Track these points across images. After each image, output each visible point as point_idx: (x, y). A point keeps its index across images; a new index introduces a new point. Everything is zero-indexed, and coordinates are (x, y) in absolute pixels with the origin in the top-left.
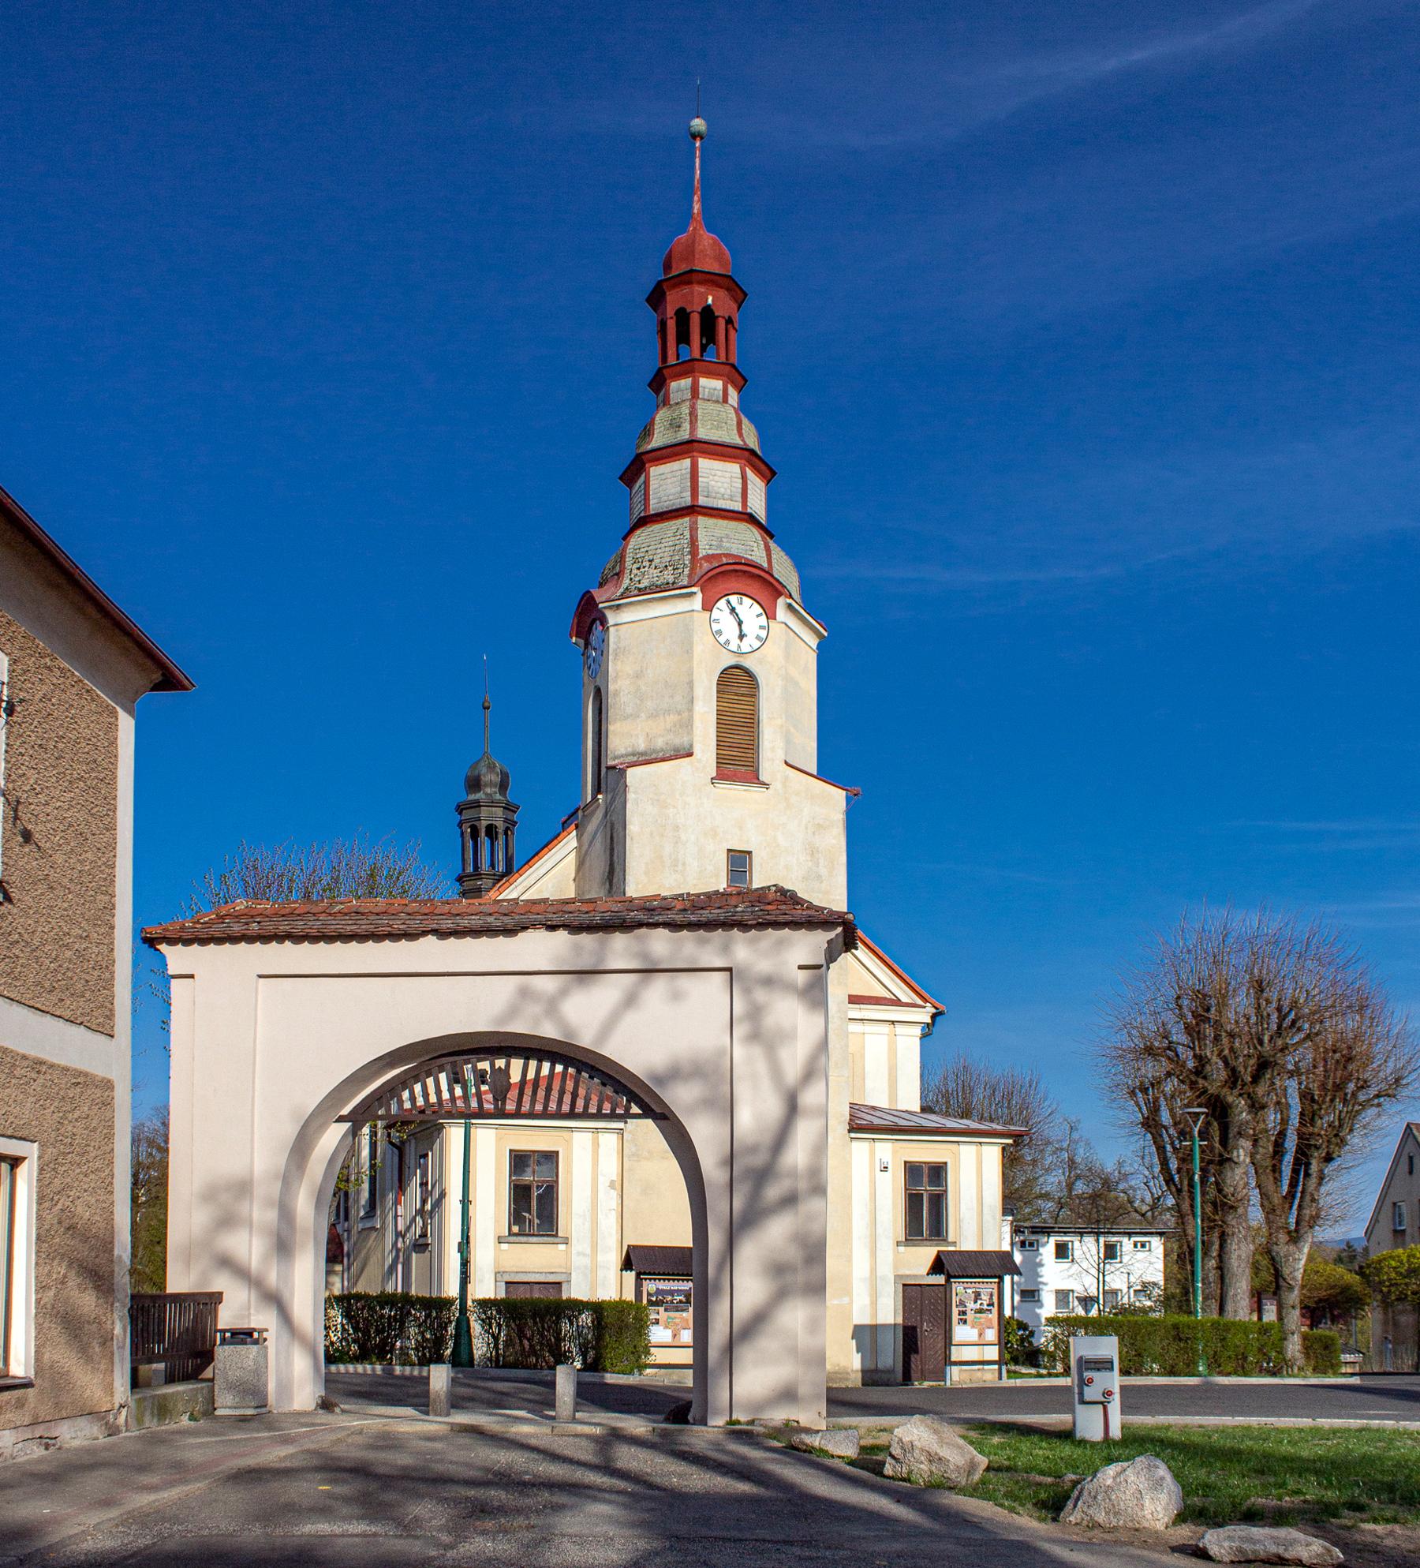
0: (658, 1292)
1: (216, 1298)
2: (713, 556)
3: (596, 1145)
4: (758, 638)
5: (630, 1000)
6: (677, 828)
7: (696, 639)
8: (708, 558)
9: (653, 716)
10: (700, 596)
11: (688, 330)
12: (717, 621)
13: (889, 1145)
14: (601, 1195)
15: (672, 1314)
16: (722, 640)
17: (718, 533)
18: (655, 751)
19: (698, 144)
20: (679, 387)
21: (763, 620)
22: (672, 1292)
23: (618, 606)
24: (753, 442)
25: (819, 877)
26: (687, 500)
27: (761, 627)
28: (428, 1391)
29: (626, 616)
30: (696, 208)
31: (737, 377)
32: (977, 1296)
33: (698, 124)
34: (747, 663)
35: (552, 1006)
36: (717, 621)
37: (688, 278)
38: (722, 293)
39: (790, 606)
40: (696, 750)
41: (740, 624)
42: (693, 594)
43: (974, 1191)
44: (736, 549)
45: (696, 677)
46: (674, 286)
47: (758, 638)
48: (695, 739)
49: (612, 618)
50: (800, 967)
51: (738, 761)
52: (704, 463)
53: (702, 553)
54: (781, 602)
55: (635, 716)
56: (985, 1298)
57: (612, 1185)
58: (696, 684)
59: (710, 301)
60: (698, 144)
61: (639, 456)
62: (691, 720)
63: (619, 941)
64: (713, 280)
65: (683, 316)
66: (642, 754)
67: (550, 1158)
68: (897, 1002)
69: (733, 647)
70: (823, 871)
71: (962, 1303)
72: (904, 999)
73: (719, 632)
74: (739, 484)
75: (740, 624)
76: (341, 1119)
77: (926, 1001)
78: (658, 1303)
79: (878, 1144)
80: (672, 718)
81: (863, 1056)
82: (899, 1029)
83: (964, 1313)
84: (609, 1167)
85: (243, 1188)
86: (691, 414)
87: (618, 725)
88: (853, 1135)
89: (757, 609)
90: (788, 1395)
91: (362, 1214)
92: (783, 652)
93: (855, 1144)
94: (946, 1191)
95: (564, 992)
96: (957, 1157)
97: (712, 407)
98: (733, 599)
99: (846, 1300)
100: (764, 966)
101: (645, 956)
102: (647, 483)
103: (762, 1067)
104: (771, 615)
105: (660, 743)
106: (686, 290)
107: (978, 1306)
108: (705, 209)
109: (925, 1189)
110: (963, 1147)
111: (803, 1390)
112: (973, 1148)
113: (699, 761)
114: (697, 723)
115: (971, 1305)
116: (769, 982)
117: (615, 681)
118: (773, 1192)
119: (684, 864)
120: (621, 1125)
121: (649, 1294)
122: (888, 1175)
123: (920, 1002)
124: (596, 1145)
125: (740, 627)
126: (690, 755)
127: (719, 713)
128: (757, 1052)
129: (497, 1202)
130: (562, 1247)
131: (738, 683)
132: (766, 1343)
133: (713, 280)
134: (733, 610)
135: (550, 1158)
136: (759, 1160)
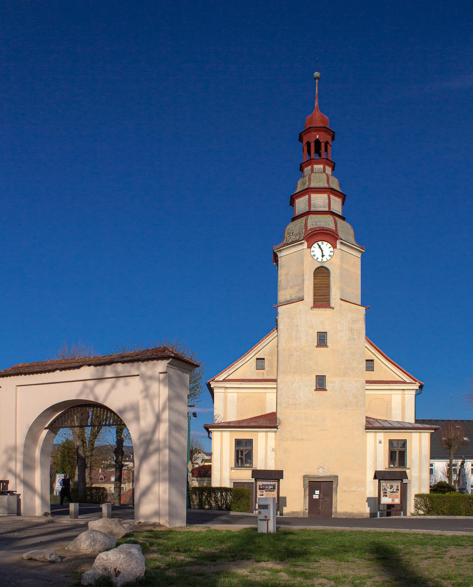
1: (7, 482)
2: (313, 228)
3: (267, 437)
4: (330, 256)
5: (113, 386)
6: (297, 326)
7: (305, 259)
8: (311, 229)
9: (292, 287)
10: (306, 244)
11: (317, 151)
12: (313, 251)
13: (382, 434)
14: (269, 453)
15: (268, 493)
16: (315, 258)
17: (316, 220)
18: (292, 300)
19: (317, 81)
20: (307, 170)
21: (332, 249)
22: (268, 485)
23: (280, 250)
24: (335, 185)
25: (354, 339)
27: (331, 252)
28: (69, 510)
29: (283, 253)
30: (316, 104)
31: (328, 162)
32: (391, 487)
33: (317, 74)
34: (325, 265)
35: (92, 389)
36: (313, 251)
37: (309, 130)
38: (323, 133)
39: (341, 243)
40: (305, 298)
42: (302, 243)
43: (418, 450)
44: (323, 225)
45: (305, 272)
46: (305, 135)
47: (330, 256)
48: (305, 294)
50: (160, 373)
51: (322, 300)
52: (313, 196)
53: (309, 228)
54: (338, 241)
55: (286, 288)
56: (395, 488)
58: (305, 275)
59: (318, 137)
60: (317, 81)
62: (303, 287)
63: (109, 368)
64: (318, 129)
66: (288, 301)
67: (250, 442)
68: (405, 382)
69: (320, 260)
71: (385, 489)
72: (408, 381)
73: (314, 255)
74: (327, 201)
75: (322, 251)
76: (46, 428)
77: (416, 381)
78: (263, 489)
79: (378, 434)
80: (297, 288)
81: (391, 402)
82: (406, 392)
83: (386, 493)
84: (272, 443)
85: (15, 449)
86: (309, 179)
88: (367, 431)
89: (329, 245)
90: (157, 514)
92: (342, 261)
93: (368, 434)
94: (406, 450)
95: (95, 385)
97: (319, 174)
98: (320, 243)
99: (363, 489)
100: (149, 373)
101: (116, 372)
103: (149, 407)
104: (334, 247)
105: (294, 297)
106: (309, 135)
107: (392, 490)
108: (320, 104)
109: (397, 449)
110: (413, 434)
111: (162, 512)
112: (373, 434)
113: (306, 302)
114: (305, 288)
115: (389, 490)
116: (151, 378)
118: (152, 448)
119: (300, 338)
121: (259, 486)
122: (382, 445)
123: (414, 382)
124: (267, 437)
125: (322, 252)
126: (303, 300)
127: (314, 284)
128: (147, 401)
131: (322, 273)
132: (151, 497)
133: (318, 129)
134: (320, 247)
135: (250, 442)
136: (148, 437)
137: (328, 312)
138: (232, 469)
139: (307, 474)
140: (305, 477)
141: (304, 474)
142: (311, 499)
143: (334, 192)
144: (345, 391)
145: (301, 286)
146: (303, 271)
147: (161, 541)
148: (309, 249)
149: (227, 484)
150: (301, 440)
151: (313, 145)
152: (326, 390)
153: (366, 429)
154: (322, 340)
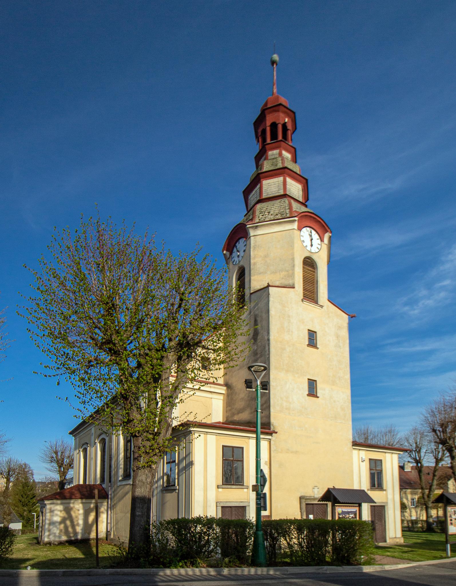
0: (343, 513)
6: (289, 316)
9: (274, 273)
22: (348, 513)
23: (257, 226)
26: (282, 192)
29: (259, 232)
34: (314, 257)
41: (312, 240)
42: (294, 221)
45: (295, 256)
46: (271, 112)
49: (252, 233)
57: (266, 463)
61: (259, 174)
65: (274, 126)
70: (341, 345)
73: (303, 241)
75: (312, 240)
87: (256, 276)
88: (354, 447)
91: (120, 478)
96: (385, 457)
102: (261, 189)
106: (276, 114)
113: (297, 291)
117: (255, 258)
119: (292, 332)
120: (270, 437)
121: (339, 514)
122: (364, 462)
126: (294, 288)
129: (217, 469)
130: (245, 490)
137: (317, 310)
138: (218, 487)
139: (303, 494)
140: (301, 498)
141: (300, 495)
142: (420, 463)
143: (306, 188)
144: (335, 402)
145: (291, 272)
146: (293, 254)
147: (418, 441)
148: (298, 232)
149: (213, 512)
150: (296, 452)
151: (280, 127)
152: (318, 397)
153: (353, 445)
154: (312, 339)
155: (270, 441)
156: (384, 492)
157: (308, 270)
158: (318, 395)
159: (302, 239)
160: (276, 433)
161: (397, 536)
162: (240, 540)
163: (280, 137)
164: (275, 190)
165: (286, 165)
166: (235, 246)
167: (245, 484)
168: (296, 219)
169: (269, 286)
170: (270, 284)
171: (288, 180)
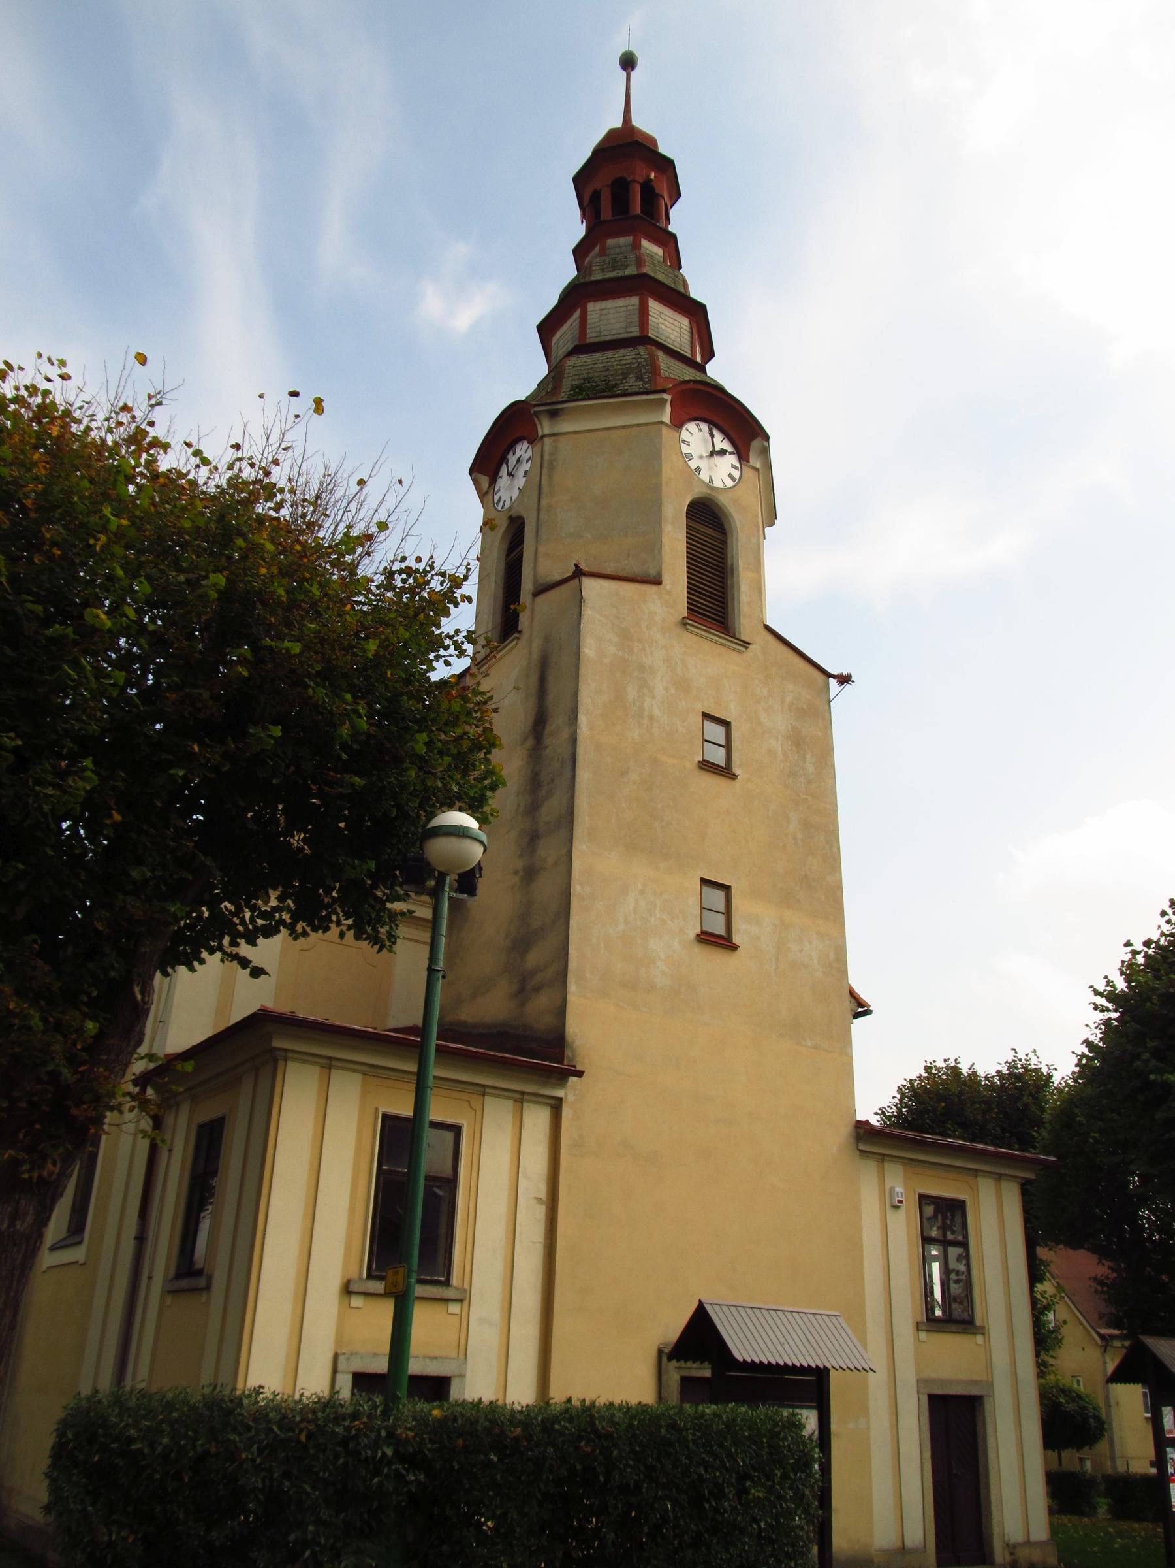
6: (642, 668)
26: (635, 332)
29: (565, 426)
113: (669, 593)
122: (902, 1213)
155: (556, 1107)
156: (979, 1339)
157: (704, 534)
158: (736, 939)
159: (685, 449)
160: (580, 1074)
161: (1033, 1538)
162: (404, 1453)
163: (637, 209)
164: (618, 326)
165: (646, 270)
166: (504, 459)
167: (455, 1281)
168: (667, 396)
169: (579, 573)
170: (583, 566)
171: (654, 306)
